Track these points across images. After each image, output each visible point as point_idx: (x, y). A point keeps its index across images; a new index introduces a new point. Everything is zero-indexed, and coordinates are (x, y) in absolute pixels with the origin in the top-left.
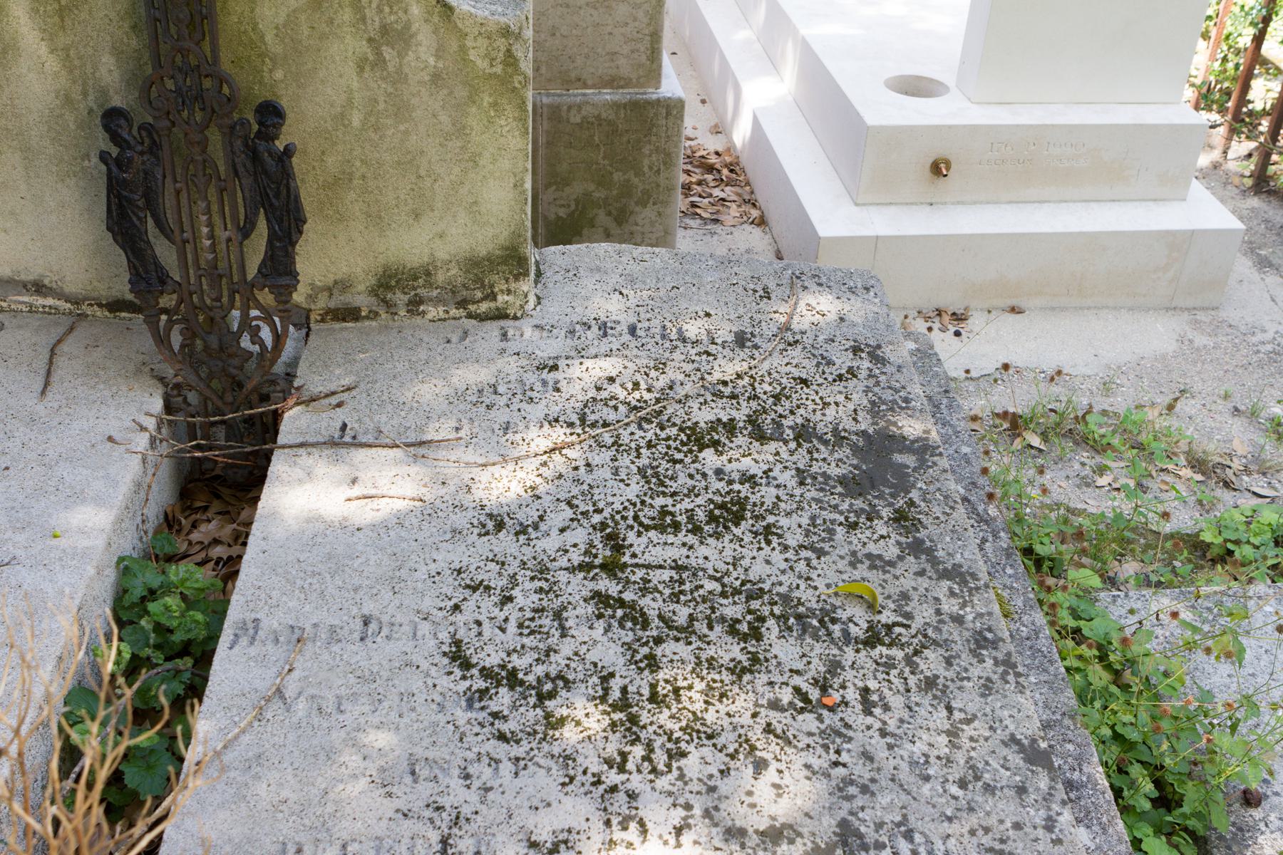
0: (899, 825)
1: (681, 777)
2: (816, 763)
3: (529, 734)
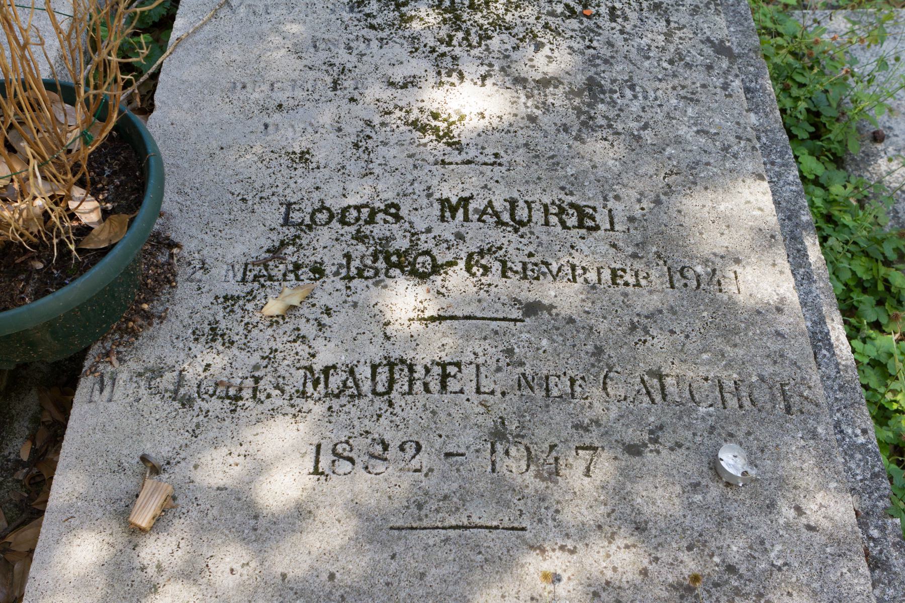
0: (626, 81)
1: (487, 49)
2: (576, 46)
3: (390, 25)
